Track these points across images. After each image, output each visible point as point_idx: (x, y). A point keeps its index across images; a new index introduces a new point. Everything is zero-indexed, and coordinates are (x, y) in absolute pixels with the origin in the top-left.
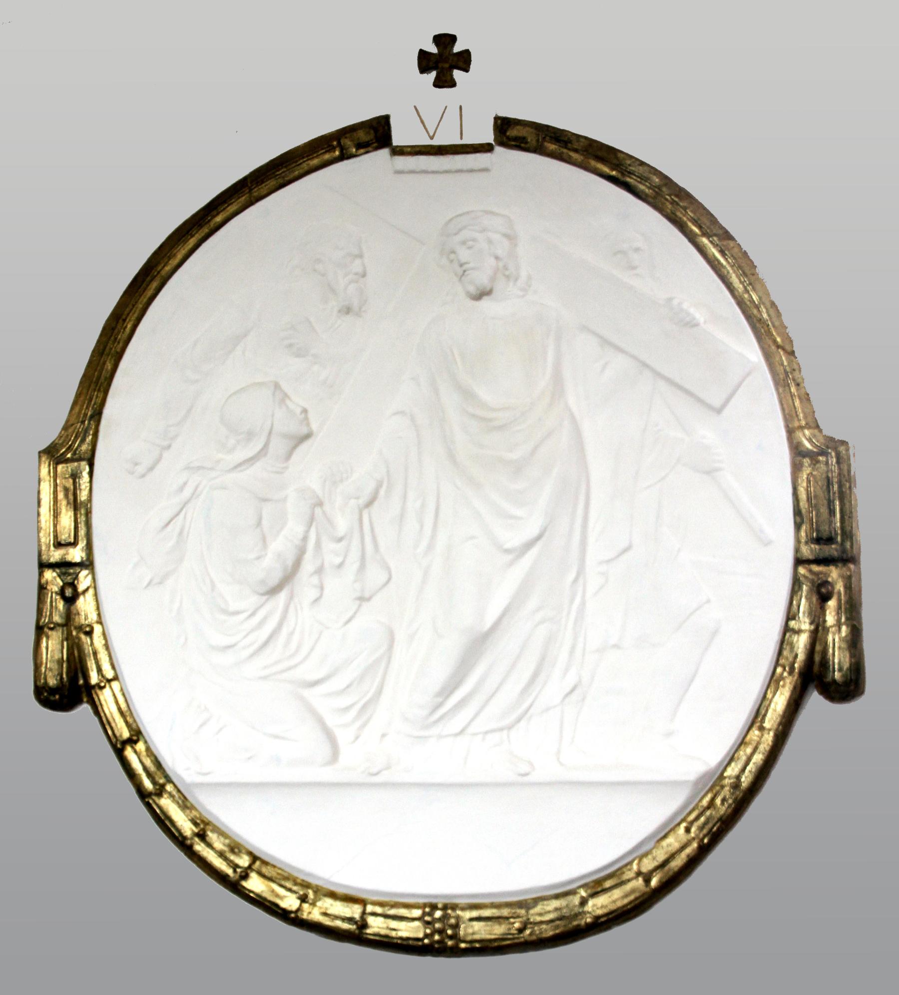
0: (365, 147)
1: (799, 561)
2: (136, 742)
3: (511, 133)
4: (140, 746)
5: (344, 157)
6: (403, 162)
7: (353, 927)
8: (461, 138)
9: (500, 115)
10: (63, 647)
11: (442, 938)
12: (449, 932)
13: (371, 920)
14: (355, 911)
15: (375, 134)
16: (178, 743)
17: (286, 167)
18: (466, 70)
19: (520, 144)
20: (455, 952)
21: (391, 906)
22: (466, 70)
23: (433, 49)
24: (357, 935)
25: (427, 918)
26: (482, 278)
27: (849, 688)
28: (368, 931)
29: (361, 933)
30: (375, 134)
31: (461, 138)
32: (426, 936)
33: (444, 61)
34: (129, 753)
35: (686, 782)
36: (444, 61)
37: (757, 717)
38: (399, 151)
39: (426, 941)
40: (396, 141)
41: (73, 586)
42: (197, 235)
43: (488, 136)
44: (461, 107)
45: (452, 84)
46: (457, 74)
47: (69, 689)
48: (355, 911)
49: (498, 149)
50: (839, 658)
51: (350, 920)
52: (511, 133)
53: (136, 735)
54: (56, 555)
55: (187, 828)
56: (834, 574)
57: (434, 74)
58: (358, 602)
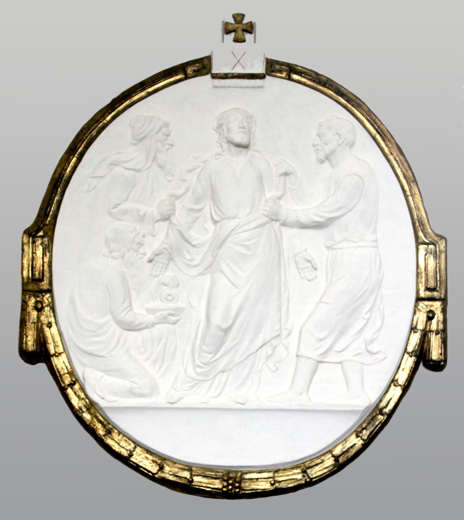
0: (198, 73)
2: (74, 384)
3: (273, 67)
4: (77, 387)
5: (187, 77)
9: (269, 57)
11: (232, 486)
12: (237, 485)
13: (195, 479)
15: (202, 67)
16: (101, 387)
21: (207, 471)
25: (226, 478)
26: (139, 312)
27: (437, 366)
28: (194, 484)
29: (190, 485)
30: (202, 67)
32: (224, 487)
35: (359, 411)
36: (239, 29)
37: (394, 381)
38: (215, 76)
39: (224, 489)
40: (215, 70)
41: (42, 303)
42: (61, 185)
43: (260, 69)
45: (244, 41)
46: (248, 36)
47: (39, 354)
49: (267, 77)
50: (435, 354)
52: (273, 67)
55: (154, 469)
56: (437, 305)
57: (245, 22)
58: (283, 177)
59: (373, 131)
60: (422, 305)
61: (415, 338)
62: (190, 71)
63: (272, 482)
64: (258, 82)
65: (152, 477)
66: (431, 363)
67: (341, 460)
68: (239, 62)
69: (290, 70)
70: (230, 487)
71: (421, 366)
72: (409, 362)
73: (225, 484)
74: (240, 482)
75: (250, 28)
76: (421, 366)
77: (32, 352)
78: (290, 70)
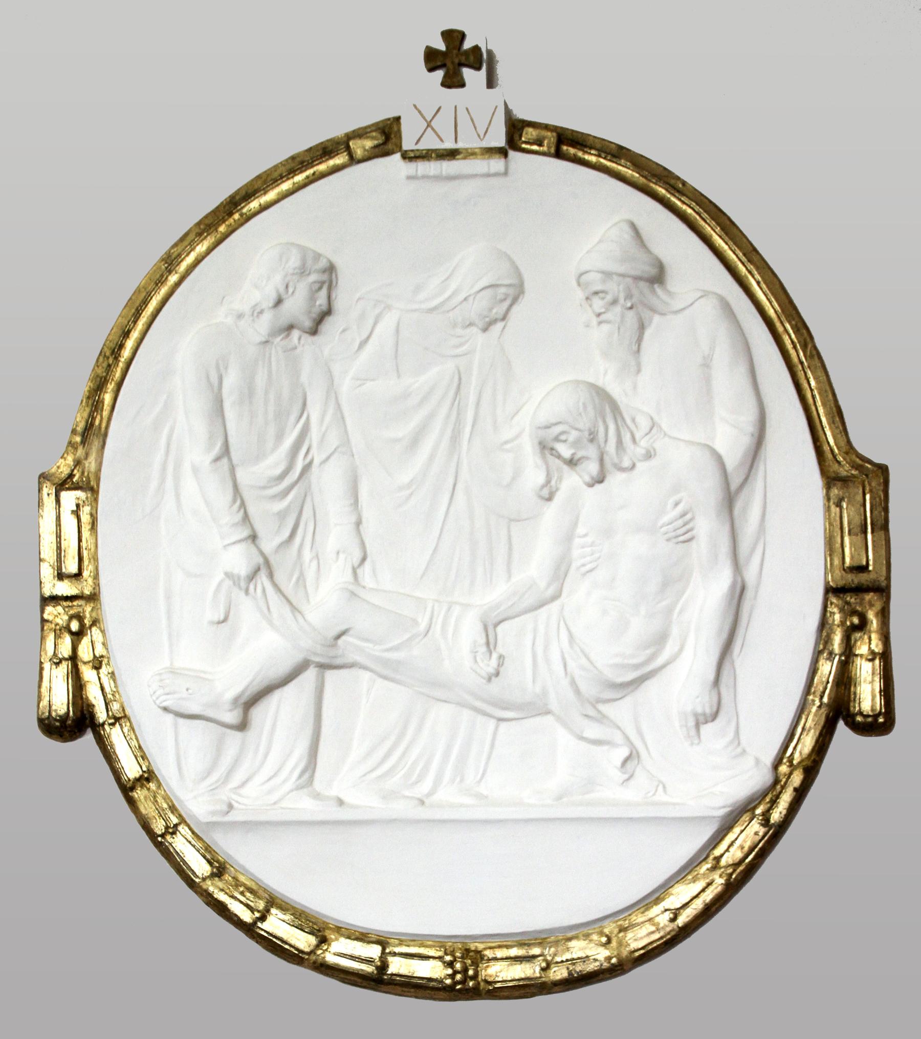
1: (830, 590)
5: (353, 160)
6: (422, 167)
7: (369, 969)
8: (456, 141)
9: (402, 121)
10: (264, 208)
14: (374, 951)
15: (387, 137)
17: (828, 705)
18: (444, 84)
19: (537, 147)
20: (475, 993)
22: (444, 84)
23: (441, 46)
24: (379, 980)
27: (879, 725)
30: (387, 137)
31: (456, 141)
33: (453, 59)
34: (139, 794)
35: (714, 817)
36: (453, 59)
39: (448, 981)
40: (408, 144)
43: (500, 141)
44: (467, 109)
45: (463, 85)
46: (440, 74)
48: (374, 951)
49: (511, 153)
50: (867, 697)
51: (368, 961)
53: (148, 777)
54: (65, 588)
59: (164, 290)
60: (56, 614)
61: (828, 669)
62: (359, 147)
63: (544, 965)
64: (497, 164)
65: (731, 889)
66: (859, 719)
67: (682, 920)
68: (428, 126)
69: (567, 144)
70: (458, 977)
71: (841, 724)
72: (813, 720)
73: (450, 971)
74: (475, 964)
75: (433, 59)
76: (841, 724)
77: (64, 719)
78: (567, 144)
